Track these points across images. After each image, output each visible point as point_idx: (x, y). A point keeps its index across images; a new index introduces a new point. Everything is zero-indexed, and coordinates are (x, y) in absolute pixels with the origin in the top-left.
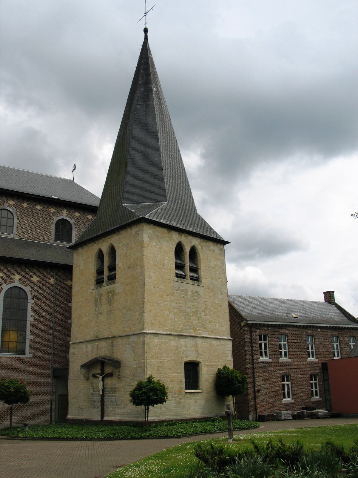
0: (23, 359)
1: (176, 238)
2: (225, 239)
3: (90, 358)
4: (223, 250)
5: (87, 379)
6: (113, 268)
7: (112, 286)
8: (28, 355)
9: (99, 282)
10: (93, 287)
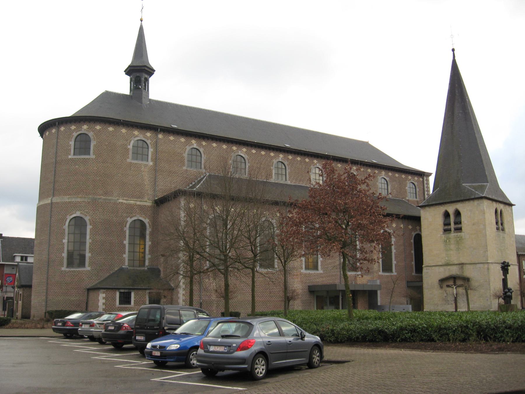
0: (391, 276)
1: (495, 205)
2: (513, 203)
3: (443, 276)
4: (512, 210)
5: (441, 287)
6: (458, 222)
7: (459, 234)
8: (394, 273)
9: (447, 231)
10: (442, 233)
